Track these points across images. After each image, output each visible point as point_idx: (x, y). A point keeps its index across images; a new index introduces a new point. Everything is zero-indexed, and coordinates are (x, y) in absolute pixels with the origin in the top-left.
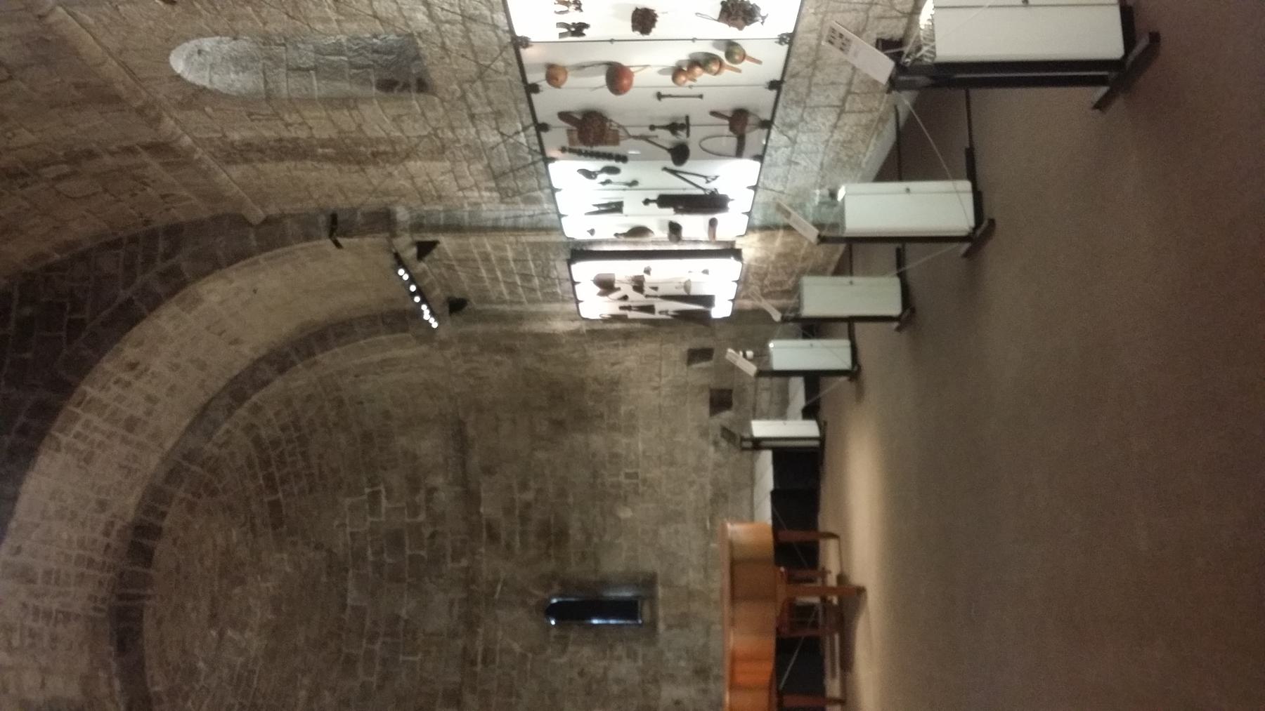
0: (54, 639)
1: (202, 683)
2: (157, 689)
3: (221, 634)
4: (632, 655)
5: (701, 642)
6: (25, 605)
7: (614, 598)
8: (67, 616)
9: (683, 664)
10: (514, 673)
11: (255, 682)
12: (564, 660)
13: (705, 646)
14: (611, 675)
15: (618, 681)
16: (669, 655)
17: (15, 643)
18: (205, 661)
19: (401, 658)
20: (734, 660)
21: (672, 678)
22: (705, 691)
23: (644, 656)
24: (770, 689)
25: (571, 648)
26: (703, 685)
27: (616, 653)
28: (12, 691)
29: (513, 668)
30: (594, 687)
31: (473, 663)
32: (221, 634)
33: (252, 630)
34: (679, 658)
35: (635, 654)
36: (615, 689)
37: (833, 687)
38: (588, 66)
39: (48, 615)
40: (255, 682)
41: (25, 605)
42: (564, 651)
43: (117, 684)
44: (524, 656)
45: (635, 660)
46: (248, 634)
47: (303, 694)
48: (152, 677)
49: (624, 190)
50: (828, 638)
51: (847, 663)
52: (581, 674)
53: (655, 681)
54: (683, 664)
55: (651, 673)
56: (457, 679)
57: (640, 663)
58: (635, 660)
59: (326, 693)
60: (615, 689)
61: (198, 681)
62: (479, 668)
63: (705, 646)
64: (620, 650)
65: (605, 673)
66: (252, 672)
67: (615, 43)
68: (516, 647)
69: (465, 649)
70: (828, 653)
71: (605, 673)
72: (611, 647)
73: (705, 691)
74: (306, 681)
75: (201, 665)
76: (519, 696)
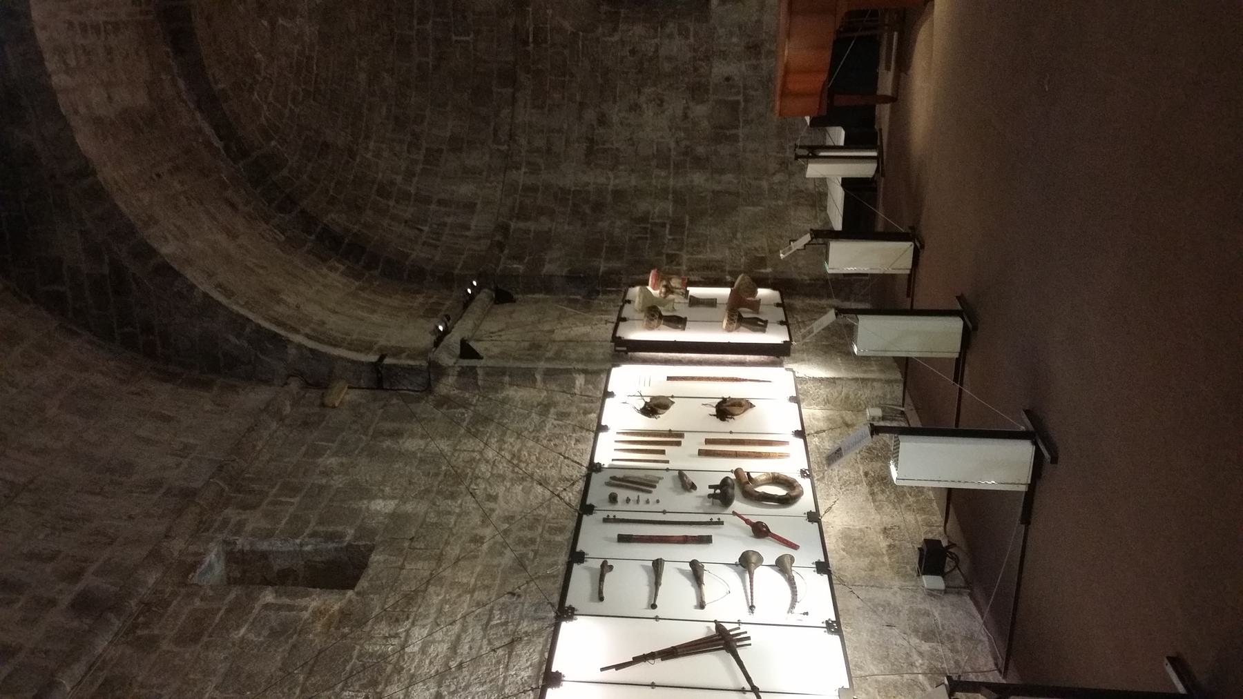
0: (109, 51)
1: (263, 73)
2: (221, 86)
3: (273, 23)
4: (684, 33)
5: (754, 18)
6: (71, 24)
7: (660, 358)
8: (117, 27)
9: (735, 40)
10: (566, 52)
11: (315, 68)
12: (616, 38)
13: (759, 21)
14: (662, 52)
15: (669, 59)
16: (721, 31)
17: (73, 63)
18: (261, 51)
19: (454, 38)
20: (787, 72)
21: (723, 55)
22: (756, 67)
23: (696, 34)
24: (821, 312)
25: (622, 27)
26: (754, 62)
27: (668, 31)
28: (82, 110)
29: (565, 47)
30: (646, 65)
31: (526, 43)
32: (273, 23)
33: (301, 16)
34: (731, 34)
35: (687, 30)
36: (667, 67)
37: (886, 84)
38: (600, 584)
39: (96, 29)
40: (315, 68)
41: (71, 24)
42: (615, 30)
43: (181, 84)
44: (575, 34)
45: (687, 38)
46: (299, 20)
47: (362, 77)
48: (213, 75)
49: (672, 397)
50: (885, 36)
51: (903, 63)
52: (633, 52)
53: (707, 58)
54: (735, 40)
55: (703, 49)
56: (511, 58)
57: (692, 40)
58: (687, 38)
59: (385, 75)
60: (667, 67)
61: (259, 73)
62: (531, 47)
63: (759, 21)
64: (671, 27)
65: (656, 51)
66: (309, 58)
67: (650, 682)
68: (567, 25)
69: (515, 28)
70: (884, 42)
71: (656, 51)
72: (663, 25)
73: (756, 68)
74: (363, 64)
75: (258, 56)
76: (572, 75)
